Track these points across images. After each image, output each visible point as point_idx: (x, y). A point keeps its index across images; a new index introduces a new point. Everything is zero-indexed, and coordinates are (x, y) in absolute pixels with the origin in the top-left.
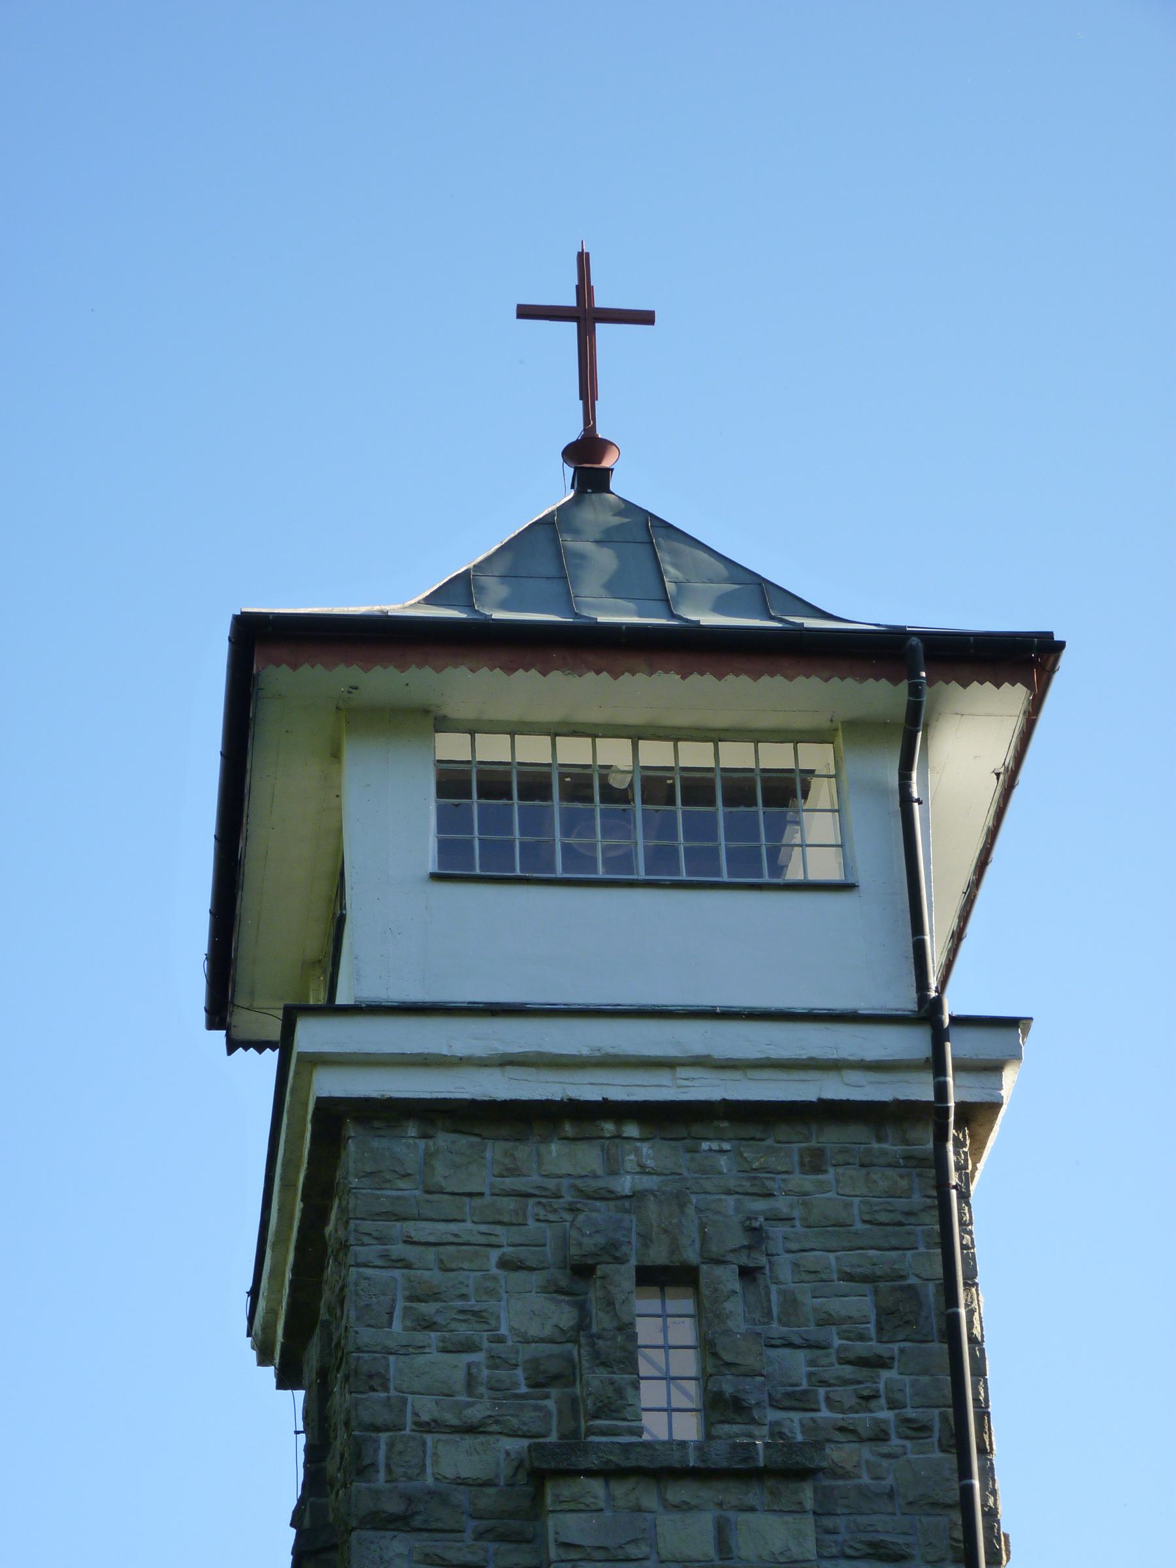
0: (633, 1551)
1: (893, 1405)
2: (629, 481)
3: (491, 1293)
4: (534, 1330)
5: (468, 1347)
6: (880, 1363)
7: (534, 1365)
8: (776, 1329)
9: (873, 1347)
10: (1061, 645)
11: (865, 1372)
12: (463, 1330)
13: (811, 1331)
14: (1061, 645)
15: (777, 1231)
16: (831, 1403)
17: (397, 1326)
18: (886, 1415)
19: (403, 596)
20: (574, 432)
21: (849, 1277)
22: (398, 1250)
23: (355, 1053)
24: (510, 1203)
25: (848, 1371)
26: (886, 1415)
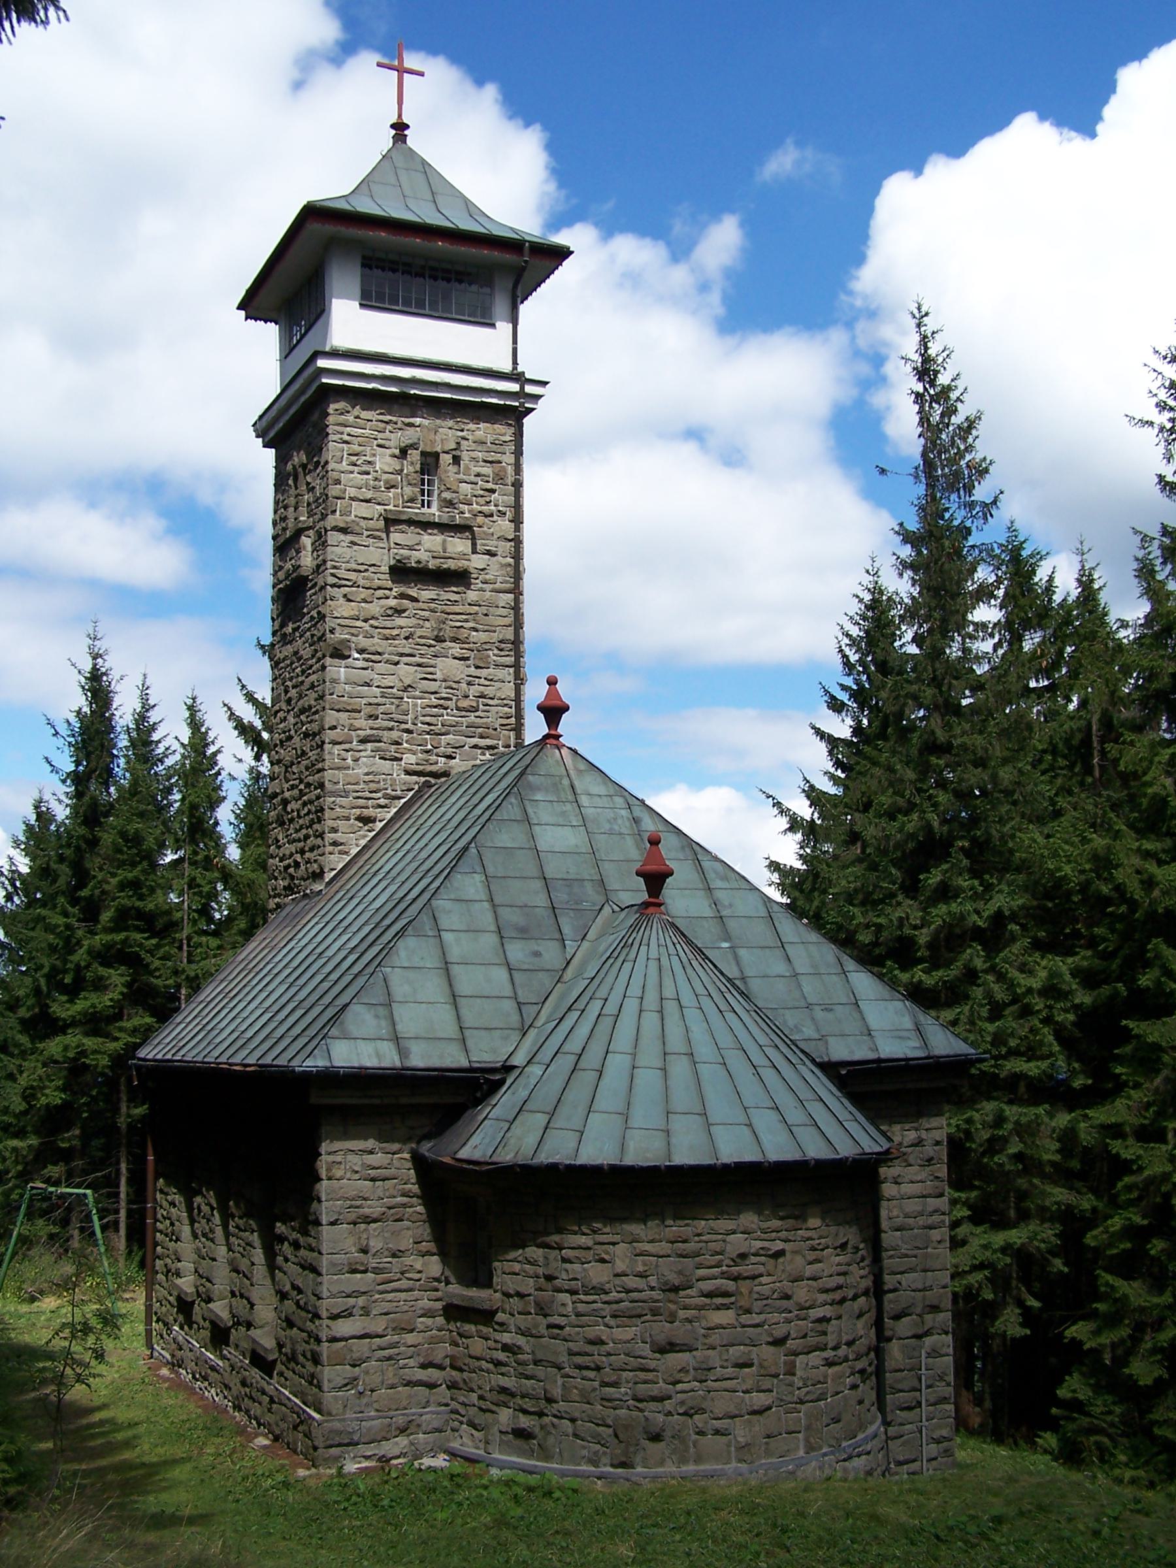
0: (417, 547)
1: (496, 506)
2: (413, 139)
3: (374, 455)
4: (387, 469)
5: (368, 473)
6: (493, 491)
7: (387, 482)
8: (461, 476)
9: (490, 486)
10: (1093, 135)
11: (487, 494)
12: (365, 468)
13: (473, 478)
14: (1093, 135)
15: (464, 443)
16: (477, 504)
17: (344, 463)
18: (493, 508)
19: (279, 391)
20: (394, 119)
21: (485, 461)
22: (346, 438)
23: (454, 1127)
24: (383, 425)
25: (482, 492)
26: (493, 508)
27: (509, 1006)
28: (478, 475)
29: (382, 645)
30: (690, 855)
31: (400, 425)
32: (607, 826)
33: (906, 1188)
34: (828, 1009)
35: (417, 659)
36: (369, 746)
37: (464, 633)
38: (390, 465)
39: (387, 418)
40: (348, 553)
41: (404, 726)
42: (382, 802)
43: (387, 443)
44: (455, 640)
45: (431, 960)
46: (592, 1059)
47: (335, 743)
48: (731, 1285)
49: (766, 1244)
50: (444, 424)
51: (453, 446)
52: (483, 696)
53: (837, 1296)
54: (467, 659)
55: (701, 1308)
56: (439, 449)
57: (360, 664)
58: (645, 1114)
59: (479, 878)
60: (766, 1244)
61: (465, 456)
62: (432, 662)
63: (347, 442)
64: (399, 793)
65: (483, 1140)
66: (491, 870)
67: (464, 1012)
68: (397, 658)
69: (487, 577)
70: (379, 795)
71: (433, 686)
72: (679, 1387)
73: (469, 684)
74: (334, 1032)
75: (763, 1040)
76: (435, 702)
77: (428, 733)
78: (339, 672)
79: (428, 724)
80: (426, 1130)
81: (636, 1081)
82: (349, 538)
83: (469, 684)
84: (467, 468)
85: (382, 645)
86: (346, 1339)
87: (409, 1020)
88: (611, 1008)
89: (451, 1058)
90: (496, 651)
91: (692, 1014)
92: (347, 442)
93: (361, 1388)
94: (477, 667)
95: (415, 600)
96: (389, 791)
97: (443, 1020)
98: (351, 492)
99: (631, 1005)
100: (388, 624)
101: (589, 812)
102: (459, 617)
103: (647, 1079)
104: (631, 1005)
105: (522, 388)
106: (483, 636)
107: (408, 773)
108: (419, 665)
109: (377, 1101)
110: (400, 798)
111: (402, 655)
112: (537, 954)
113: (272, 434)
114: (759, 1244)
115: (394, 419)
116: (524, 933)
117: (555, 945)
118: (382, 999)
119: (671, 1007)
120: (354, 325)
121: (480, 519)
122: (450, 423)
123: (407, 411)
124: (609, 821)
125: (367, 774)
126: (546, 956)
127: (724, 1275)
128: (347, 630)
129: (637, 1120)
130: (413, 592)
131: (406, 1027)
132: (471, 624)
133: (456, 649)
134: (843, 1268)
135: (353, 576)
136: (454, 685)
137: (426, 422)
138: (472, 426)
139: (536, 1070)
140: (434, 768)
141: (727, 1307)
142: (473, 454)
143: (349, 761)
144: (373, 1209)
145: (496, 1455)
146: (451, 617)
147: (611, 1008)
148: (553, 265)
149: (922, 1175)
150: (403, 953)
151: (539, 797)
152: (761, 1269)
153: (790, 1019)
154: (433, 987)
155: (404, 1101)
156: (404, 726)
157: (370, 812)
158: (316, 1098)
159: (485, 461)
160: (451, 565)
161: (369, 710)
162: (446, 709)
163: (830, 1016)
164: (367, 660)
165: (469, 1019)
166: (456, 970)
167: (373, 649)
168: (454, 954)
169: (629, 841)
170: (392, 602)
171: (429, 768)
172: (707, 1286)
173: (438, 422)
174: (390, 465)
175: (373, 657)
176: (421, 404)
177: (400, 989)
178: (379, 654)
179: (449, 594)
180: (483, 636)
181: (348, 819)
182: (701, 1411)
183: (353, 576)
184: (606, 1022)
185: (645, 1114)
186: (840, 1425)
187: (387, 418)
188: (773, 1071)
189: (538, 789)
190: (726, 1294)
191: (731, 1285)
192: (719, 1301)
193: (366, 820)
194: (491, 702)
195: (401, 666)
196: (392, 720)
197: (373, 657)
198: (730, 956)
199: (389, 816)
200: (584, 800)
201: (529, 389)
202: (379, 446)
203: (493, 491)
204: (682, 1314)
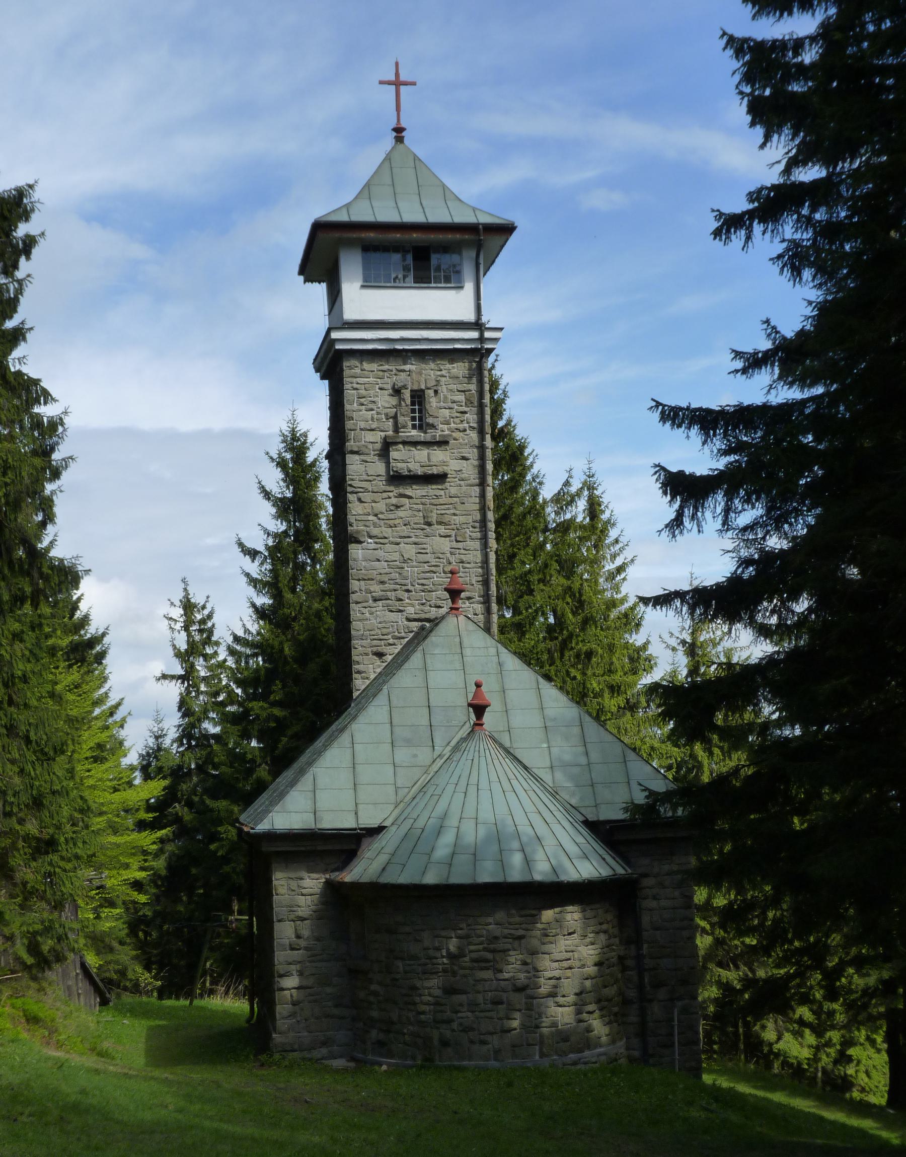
1: (468, 423)
3: (377, 396)
4: (387, 405)
5: (372, 410)
6: (465, 413)
9: (464, 409)
12: (371, 406)
21: (459, 391)
22: (355, 386)
25: (458, 415)
27: (391, 789)
28: (454, 402)
29: (388, 532)
31: (394, 371)
33: (664, 903)
35: (413, 539)
36: (380, 603)
37: (446, 519)
38: (388, 402)
39: (386, 367)
40: (361, 468)
41: (404, 588)
42: (391, 641)
43: (385, 386)
44: (440, 523)
47: (357, 603)
48: (489, 956)
49: (512, 932)
50: (427, 367)
51: (434, 383)
52: (462, 562)
53: (565, 964)
54: (449, 536)
55: (472, 969)
56: (423, 387)
57: (373, 546)
60: (512, 932)
61: (443, 389)
62: (424, 540)
63: (357, 389)
64: (403, 634)
65: (364, 869)
68: (399, 540)
69: (463, 476)
70: (390, 637)
72: (460, 1015)
73: (451, 553)
76: (427, 568)
77: (423, 591)
78: (357, 553)
79: (423, 585)
80: (336, 865)
82: (362, 457)
84: (445, 397)
85: (388, 532)
86: (289, 989)
87: (325, 800)
89: (347, 822)
90: (471, 529)
92: (357, 389)
93: (299, 1019)
94: (457, 541)
95: (410, 497)
96: (396, 634)
97: (346, 799)
98: (362, 425)
99: (450, 788)
100: (392, 516)
102: (443, 507)
104: (450, 788)
105: (482, 335)
106: (462, 519)
107: (409, 620)
108: (415, 544)
109: (303, 849)
110: (403, 638)
111: (401, 537)
112: (415, 756)
114: (506, 931)
115: (390, 368)
116: (409, 743)
117: (430, 749)
118: (311, 788)
119: (472, 790)
120: (363, 301)
121: (456, 434)
122: (432, 365)
123: (400, 361)
125: (380, 623)
127: (485, 949)
128: (363, 523)
130: (409, 492)
132: (452, 511)
133: (442, 530)
134: (572, 948)
135: (364, 484)
136: (441, 556)
137: (413, 367)
138: (448, 366)
139: (394, 828)
140: (427, 616)
141: (487, 969)
142: (450, 387)
143: (367, 615)
145: (370, 1057)
146: (438, 507)
148: (504, 238)
149: (677, 893)
152: (509, 946)
154: (344, 778)
155: (319, 848)
156: (406, 588)
158: (266, 848)
159: (459, 391)
160: (435, 471)
161: (379, 577)
162: (435, 573)
164: (376, 543)
167: (380, 535)
168: (360, 758)
170: (394, 501)
172: (474, 955)
173: (423, 366)
174: (388, 402)
175: (381, 541)
176: (410, 354)
178: (386, 538)
179: (431, 490)
180: (462, 519)
181: (367, 654)
182: (472, 1029)
183: (364, 484)
186: (568, 1044)
187: (386, 367)
190: (487, 961)
191: (489, 956)
192: (483, 965)
193: (380, 655)
194: (468, 565)
195: (402, 545)
196: (396, 584)
197: (381, 541)
199: (396, 651)
200: (467, 652)
201: (487, 335)
202: (381, 389)
203: (465, 413)
204: (462, 972)
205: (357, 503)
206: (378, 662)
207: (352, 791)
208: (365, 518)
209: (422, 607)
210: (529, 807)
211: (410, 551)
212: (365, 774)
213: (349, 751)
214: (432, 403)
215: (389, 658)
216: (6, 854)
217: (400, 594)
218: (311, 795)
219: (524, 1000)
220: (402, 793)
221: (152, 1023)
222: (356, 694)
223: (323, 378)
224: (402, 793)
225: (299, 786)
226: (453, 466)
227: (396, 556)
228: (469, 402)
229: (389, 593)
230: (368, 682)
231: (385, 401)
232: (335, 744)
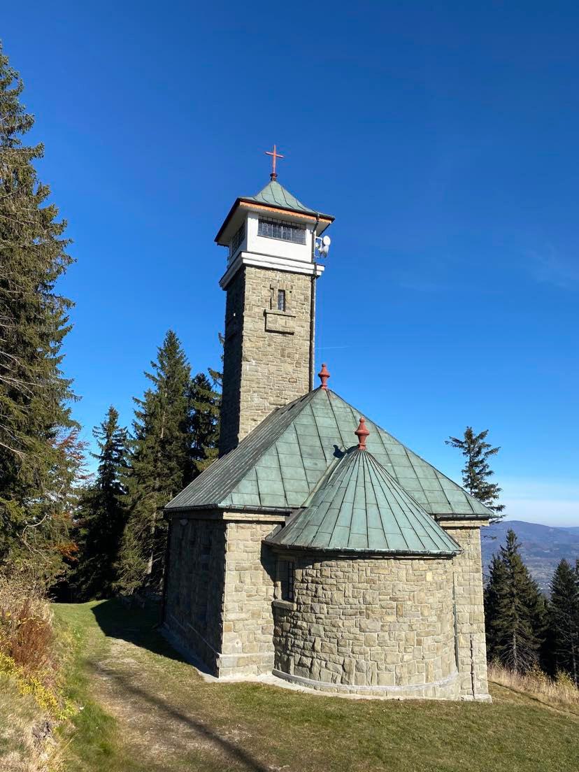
9: (303, 302)
19: (227, 270)
27: (304, 483)
30: (375, 430)
32: (343, 419)
34: (430, 491)
42: (261, 414)
45: (275, 465)
46: (337, 505)
58: (359, 528)
59: (294, 435)
61: (294, 291)
66: (299, 432)
67: (286, 484)
71: (281, 373)
73: (293, 373)
74: (234, 490)
75: (407, 501)
81: (354, 514)
83: (293, 373)
84: (295, 296)
88: (344, 485)
91: (378, 489)
97: (278, 487)
98: (253, 303)
99: (353, 484)
101: (336, 413)
103: (360, 513)
104: (353, 484)
113: (226, 284)
118: (255, 478)
124: (344, 416)
126: (319, 465)
129: (355, 529)
131: (263, 490)
144: (247, 565)
147: (344, 485)
150: (264, 462)
151: (318, 407)
153: (417, 495)
154: (274, 475)
157: (255, 418)
163: (432, 495)
165: (288, 487)
166: (284, 469)
168: (283, 462)
169: (352, 424)
171: (278, 403)
177: (262, 474)
184: (343, 490)
185: (359, 528)
188: (412, 532)
189: (317, 404)
198: (392, 469)
199: (263, 420)
200: (335, 409)
205: (248, 341)
206: (254, 423)
207: (281, 483)
208: (251, 349)
209: (277, 398)
210: (407, 501)
211: (273, 369)
212: (288, 472)
213: (276, 458)
214: (288, 296)
215: (259, 423)
216: (3, 752)
217: (267, 390)
218: (254, 483)
219: (416, 638)
220: (312, 486)
221: (94, 603)
222: (240, 441)
223: (224, 289)
224: (312, 486)
225: (247, 477)
226: (297, 330)
227: (266, 371)
228: (306, 299)
229: (261, 389)
230: (247, 434)
231: (266, 293)
232: (267, 453)
